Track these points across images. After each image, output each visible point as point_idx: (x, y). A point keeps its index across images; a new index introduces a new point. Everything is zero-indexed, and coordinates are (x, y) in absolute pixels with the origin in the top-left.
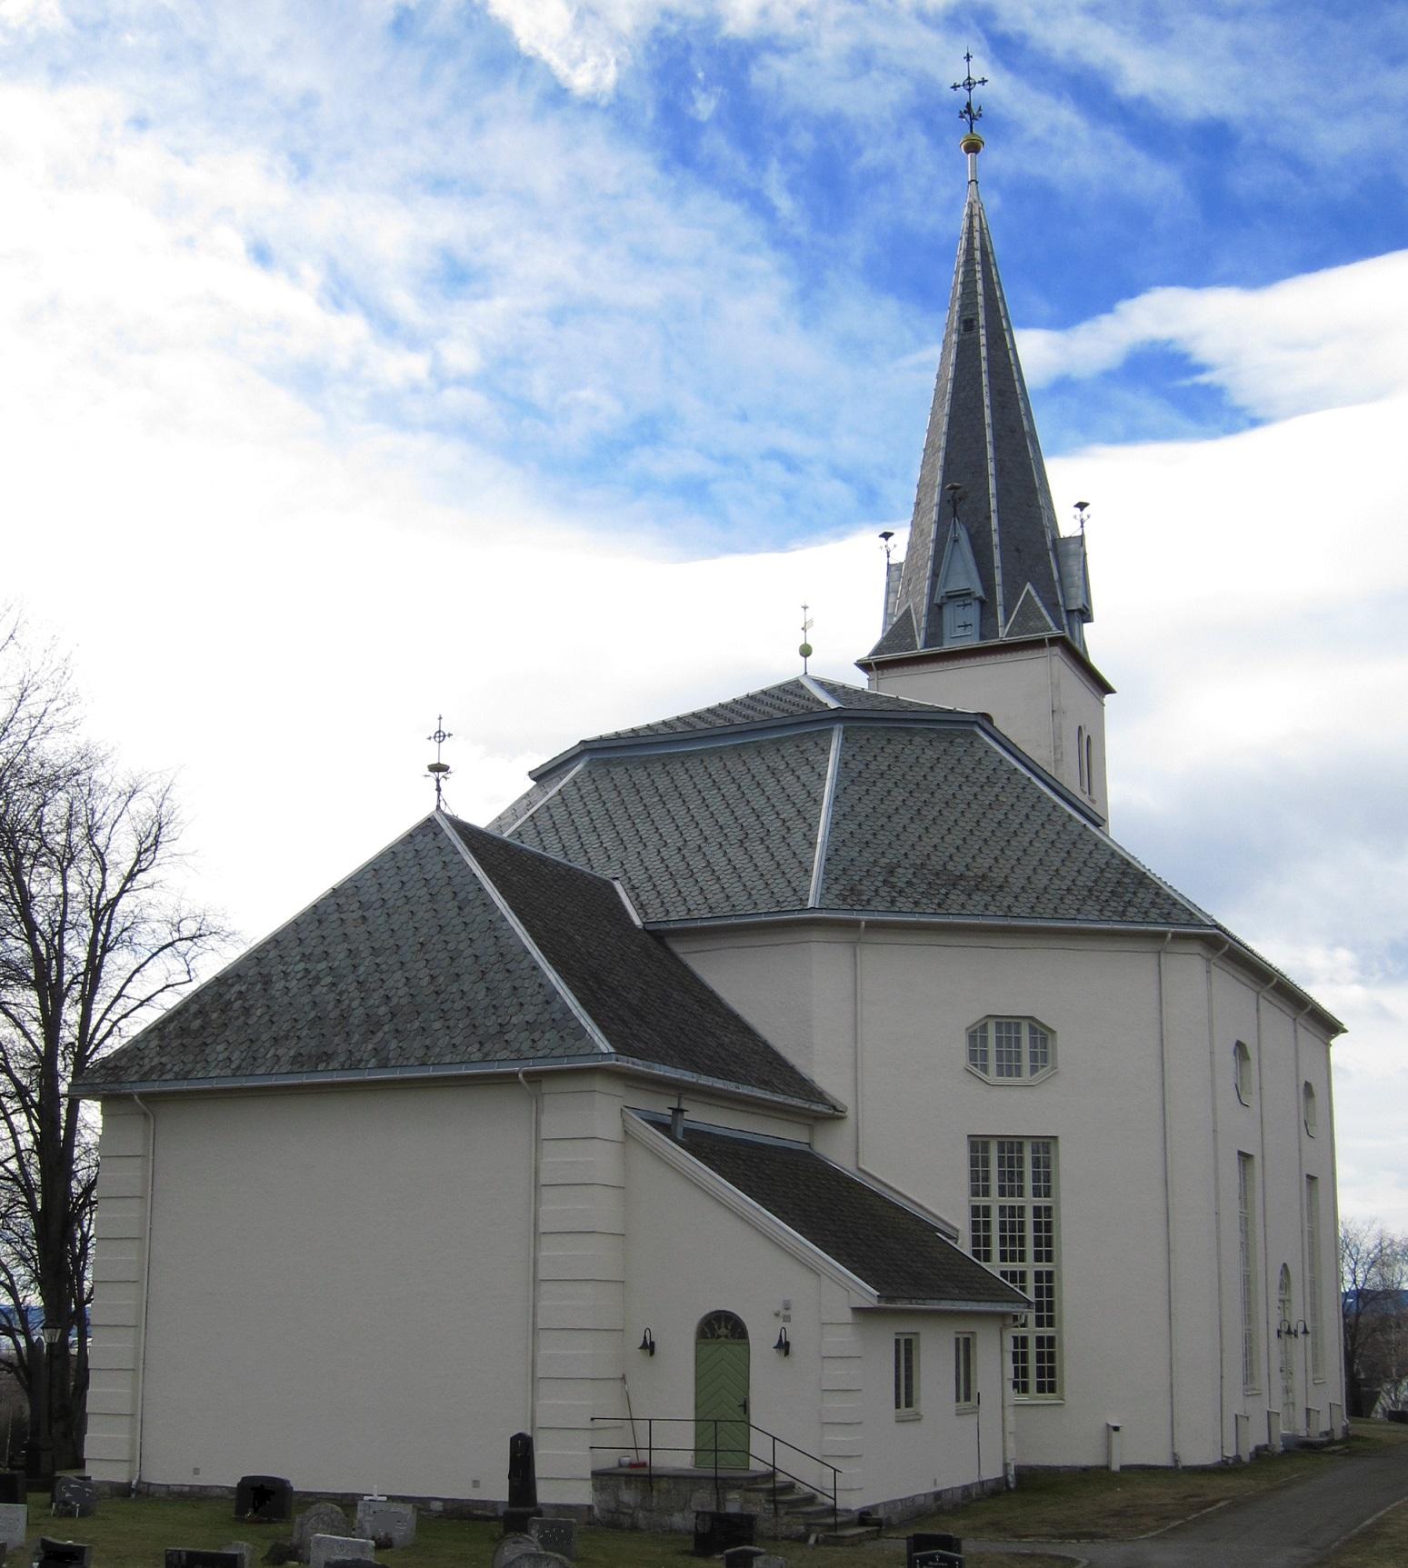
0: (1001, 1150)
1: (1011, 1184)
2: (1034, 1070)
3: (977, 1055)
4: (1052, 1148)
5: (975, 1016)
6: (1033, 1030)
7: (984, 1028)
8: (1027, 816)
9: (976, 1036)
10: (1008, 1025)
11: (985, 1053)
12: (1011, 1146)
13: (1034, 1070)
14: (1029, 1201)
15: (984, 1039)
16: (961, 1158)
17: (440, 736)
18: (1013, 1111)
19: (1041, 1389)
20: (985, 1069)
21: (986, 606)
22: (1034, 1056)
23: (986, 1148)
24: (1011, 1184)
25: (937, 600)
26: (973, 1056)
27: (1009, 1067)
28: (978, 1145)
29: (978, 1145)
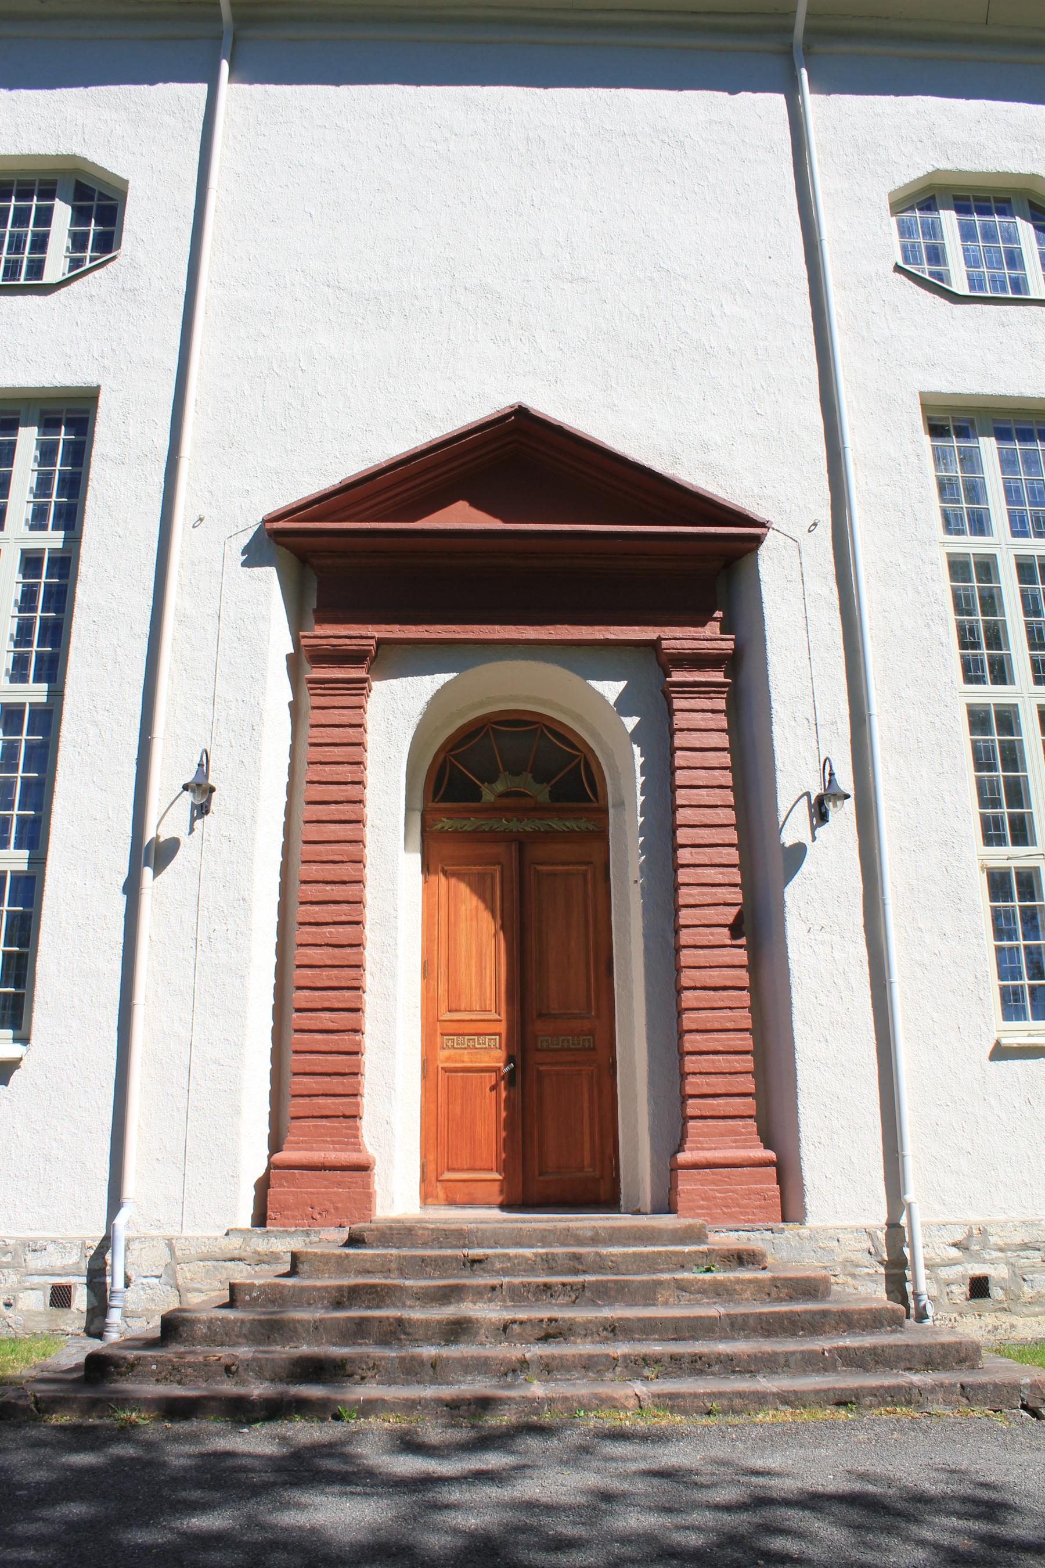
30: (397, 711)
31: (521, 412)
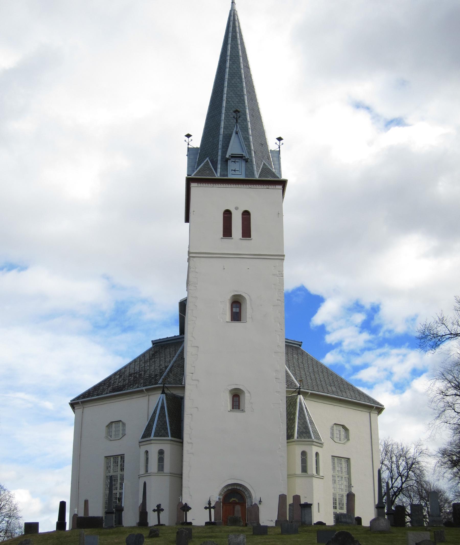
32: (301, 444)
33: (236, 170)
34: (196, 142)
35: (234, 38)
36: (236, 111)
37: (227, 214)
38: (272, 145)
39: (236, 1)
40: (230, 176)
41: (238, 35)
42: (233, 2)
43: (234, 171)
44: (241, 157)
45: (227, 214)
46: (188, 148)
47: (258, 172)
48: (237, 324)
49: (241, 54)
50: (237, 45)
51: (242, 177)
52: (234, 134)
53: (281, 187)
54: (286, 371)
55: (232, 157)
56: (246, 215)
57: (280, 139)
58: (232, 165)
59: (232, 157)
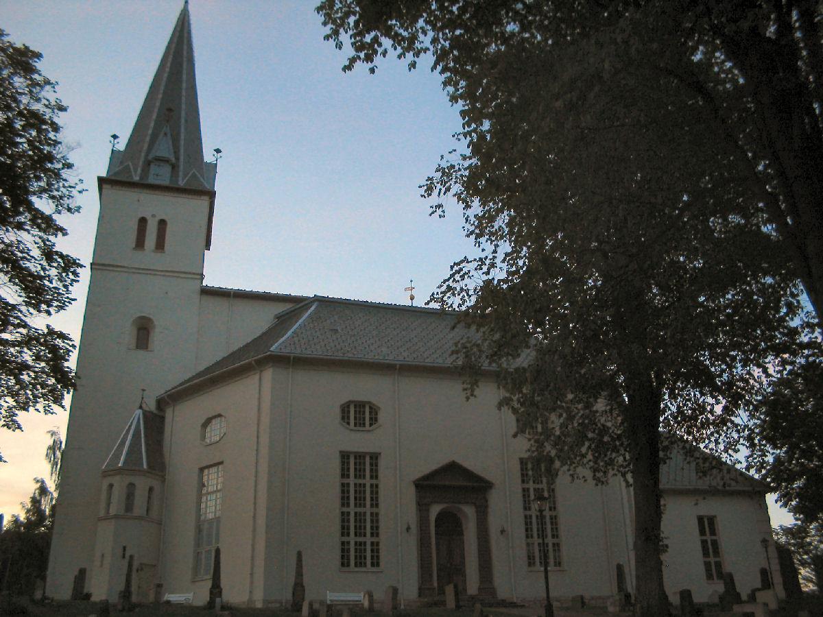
0: (355, 458)
1: (360, 473)
2: (371, 425)
3: (345, 416)
4: (379, 458)
5: (344, 400)
6: (370, 408)
7: (348, 407)
8: (380, 325)
9: (345, 409)
10: (360, 406)
11: (349, 418)
12: (360, 457)
13: (371, 425)
14: (358, 461)
15: (349, 412)
16: (336, 463)
17: (372, 71)
18: (359, 442)
19: (373, 565)
20: (348, 423)
21: (174, 167)
22: (371, 419)
23: (348, 457)
24: (360, 473)
25: (150, 157)
26: (343, 418)
27: (360, 423)
28: (345, 456)
29: (345, 456)
30: (435, 510)
31: (454, 462)
32: (236, 381)
33: (161, 175)
34: (121, 145)
35: (182, 31)
36: (170, 110)
37: (143, 221)
38: (208, 157)
39: (189, 2)
40: (151, 180)
41: (185, 47)
42: (186, 2)
43: (157, 175)
44: (167, 161)
45: (143, 221)
46: (112, 150)
47: (185, 176)
48: (141, 353)
49: (185, 53)
50: (179, 73)
51: (166, 183)
52: (162, 135)
53: (206, 198)
54: (444, 194)
55: (156, 160)
56: (162, 223)
57: (218, 151)
58: (154, 169)
59: (156, 160)
